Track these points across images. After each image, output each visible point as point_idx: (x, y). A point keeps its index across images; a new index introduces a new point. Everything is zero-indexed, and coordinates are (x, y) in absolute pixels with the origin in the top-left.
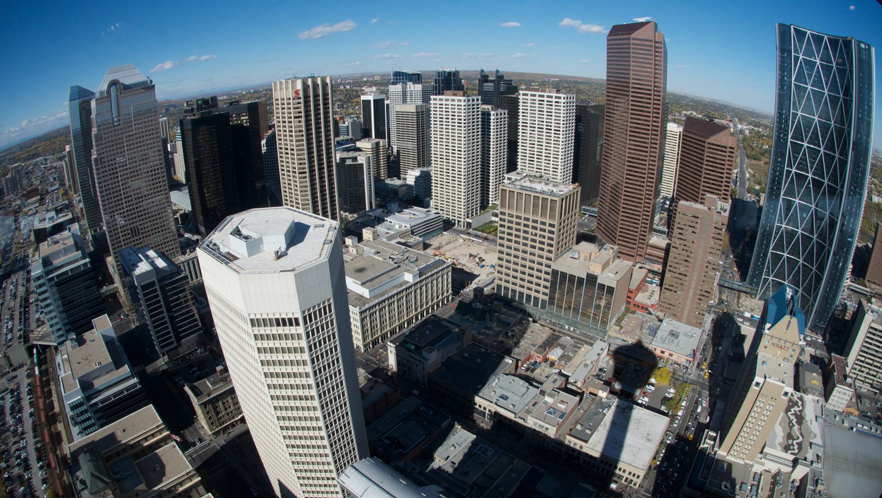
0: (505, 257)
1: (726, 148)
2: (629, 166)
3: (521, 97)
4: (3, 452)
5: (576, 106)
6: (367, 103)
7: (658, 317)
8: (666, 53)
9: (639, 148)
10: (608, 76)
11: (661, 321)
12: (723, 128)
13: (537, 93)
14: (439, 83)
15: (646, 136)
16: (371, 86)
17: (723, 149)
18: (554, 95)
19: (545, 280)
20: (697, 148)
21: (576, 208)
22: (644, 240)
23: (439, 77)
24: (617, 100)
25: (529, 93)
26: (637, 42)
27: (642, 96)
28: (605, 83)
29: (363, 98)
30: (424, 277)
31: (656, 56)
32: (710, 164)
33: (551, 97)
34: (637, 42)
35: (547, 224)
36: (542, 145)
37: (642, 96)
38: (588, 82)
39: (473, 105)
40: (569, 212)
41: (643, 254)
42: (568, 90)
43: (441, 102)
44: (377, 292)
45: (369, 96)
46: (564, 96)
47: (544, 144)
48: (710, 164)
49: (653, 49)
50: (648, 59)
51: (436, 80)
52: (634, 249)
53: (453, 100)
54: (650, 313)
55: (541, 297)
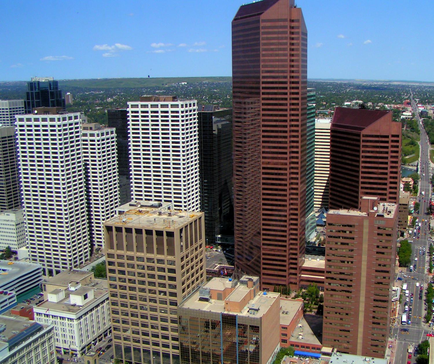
0: (119, 308)
1: (387, 137)
4: (60, 361)
5: (198, 114)
8: (305, 34)
12: (383, 113)
13: (149, 103)
14: (33, 99)
15: (284, 140)
17: (384, 139)
19: (173, 330)
20: (276, 190)
21: (201, 238)
22: (296, 264)
23: (32, 89)
24: (247, 100)
26: (268, 24)
27: (276, 91)
28: (231, 81)
30: (16, 349)
32: (368, 160)
34: (268, 24)
37: (276, 91)
40: (196, 241)
41: (297, 281)
42: (186, 96)
43: (37, 123)
44: (12, 343)
46: (182, 103)
48: (368, 160)
49: (288, 30)
50: (281, 44)
51: (28, 93)
52: (285, 276)
55: (171, 351)
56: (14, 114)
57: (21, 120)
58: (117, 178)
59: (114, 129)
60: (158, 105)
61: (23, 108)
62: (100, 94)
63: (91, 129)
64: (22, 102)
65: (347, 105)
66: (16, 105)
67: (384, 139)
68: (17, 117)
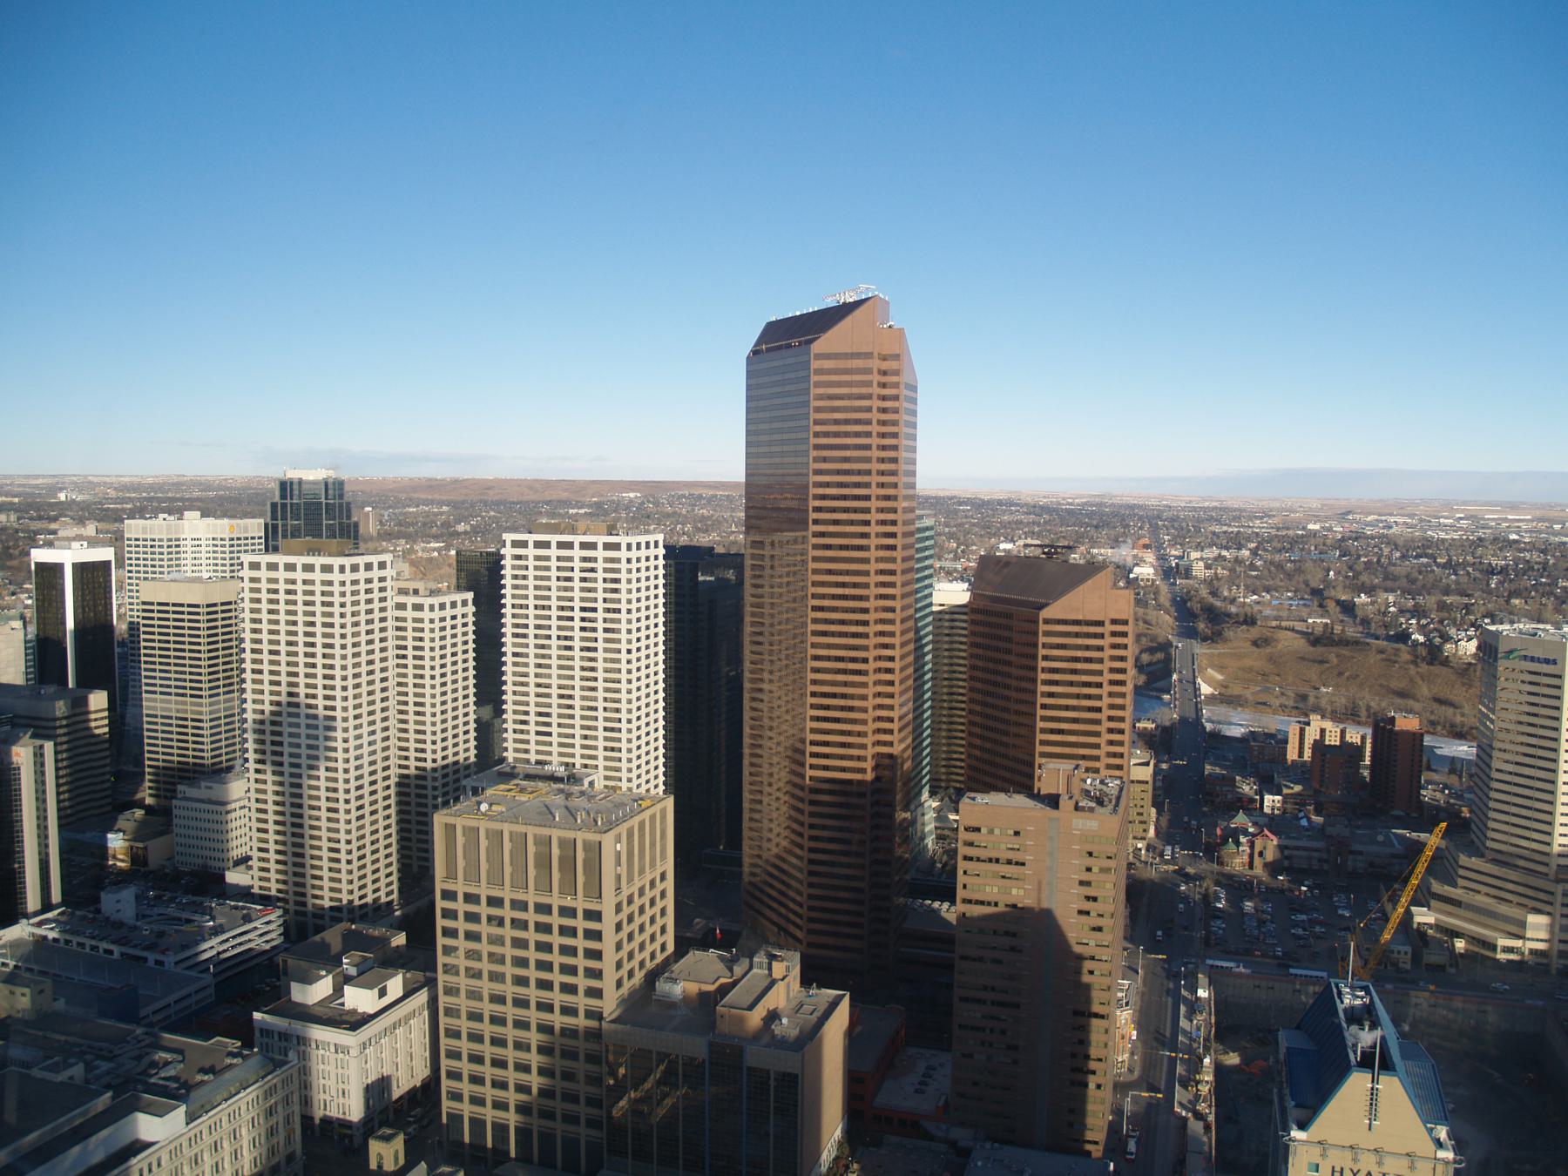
1: (1101, 623)
2: (818, 719)
3: (508, 551)
6: (51, 573)
7: (953, 1144)
9: (841, 665)
10: (747, 475)
11: (965, 1153)
12: (1093, 568)
16: (81, 521)
17: (1092, 629)
18: (601, 539)
25: (532, 538)
29: (39, 555)
31: (760, 847)
33: (593, 546)
35: (557, 987)
36: (561, 696)
38: (693, 495)
39: (369, 581)
40: (642, 871)
45: (68, 555)
47: (577, 634)
51: (274, 505)
53: (309, 568)
54: (931, 1138)
56: (239, 552)
57: (255, 566)
58: (472, 708)
59: (470, 596)
60: (619, 544)
61: (260, 538)
62: (442, 514)
63: (416, 592)
64: (259, 524)
65: (1005, 550)
66: (246, 531)
67: (1092, 629)
68: (247, 559)
